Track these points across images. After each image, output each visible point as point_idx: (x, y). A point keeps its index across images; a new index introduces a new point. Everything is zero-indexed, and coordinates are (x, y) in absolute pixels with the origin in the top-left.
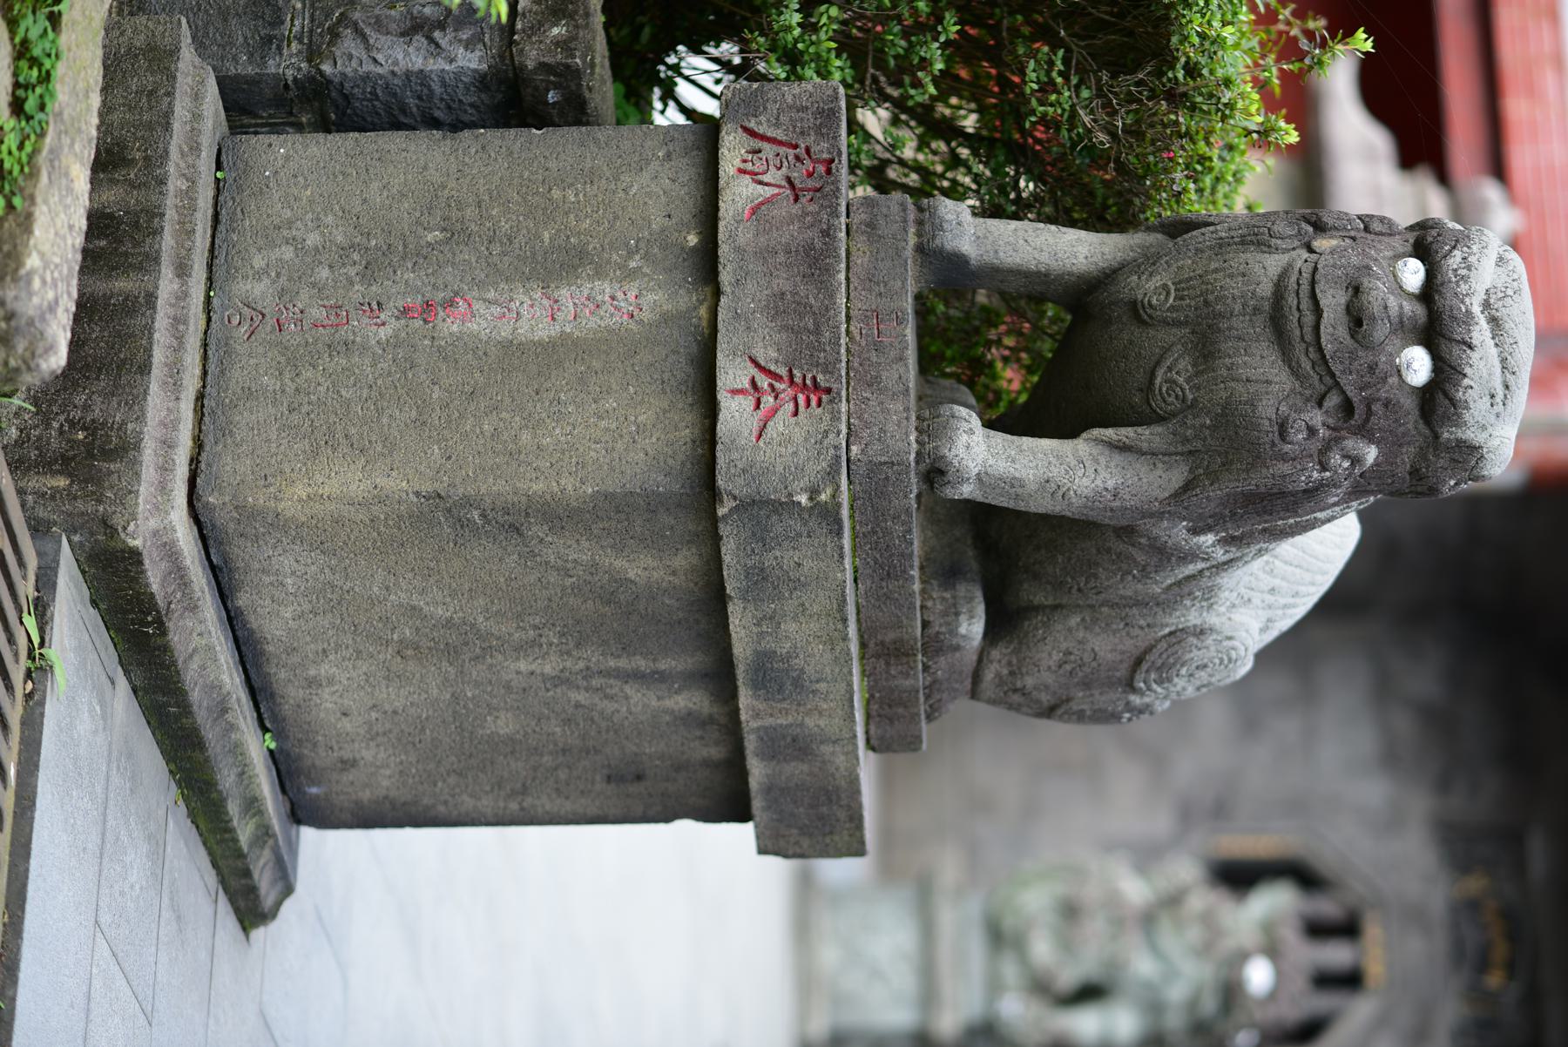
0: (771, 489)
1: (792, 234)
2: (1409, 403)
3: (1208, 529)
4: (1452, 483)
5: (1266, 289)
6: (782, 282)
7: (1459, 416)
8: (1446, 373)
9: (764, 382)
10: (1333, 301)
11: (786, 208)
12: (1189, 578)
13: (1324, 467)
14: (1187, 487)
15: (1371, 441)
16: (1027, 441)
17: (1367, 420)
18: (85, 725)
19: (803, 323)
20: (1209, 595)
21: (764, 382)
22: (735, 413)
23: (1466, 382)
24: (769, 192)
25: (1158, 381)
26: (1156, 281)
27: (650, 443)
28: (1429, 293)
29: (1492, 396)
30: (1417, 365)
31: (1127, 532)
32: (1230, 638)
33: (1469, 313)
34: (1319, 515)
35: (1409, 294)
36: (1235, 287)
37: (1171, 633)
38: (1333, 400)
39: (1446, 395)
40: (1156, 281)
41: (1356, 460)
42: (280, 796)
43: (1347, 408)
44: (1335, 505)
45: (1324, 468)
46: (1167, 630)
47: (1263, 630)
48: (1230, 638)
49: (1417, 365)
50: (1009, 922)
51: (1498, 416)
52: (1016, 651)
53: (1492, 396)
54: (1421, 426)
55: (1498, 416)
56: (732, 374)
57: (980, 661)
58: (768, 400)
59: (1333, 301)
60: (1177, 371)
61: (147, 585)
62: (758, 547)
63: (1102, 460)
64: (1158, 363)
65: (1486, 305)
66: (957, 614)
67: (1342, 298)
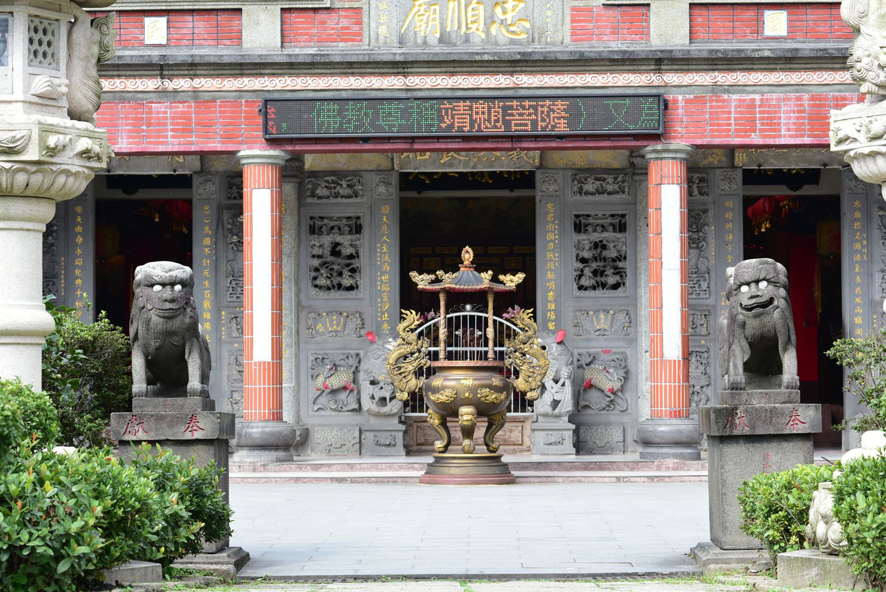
0: (217, 427)
1: (152, 424)
2: (185, 290)
5: (162, 320)
6: (165, 426)
9: (190, 429)
10: (168, 305)
11: (145, 425)
16: (190, 373)
18: (249, 571)
19: (174, 421)
21: (190, 429)
22: (198, 435)
24: (141, 429)
26: (153, 343)
27: (202, 454)
28: (164, 285)
30: (178, 287)
36: (160, 327)
40: (153, 343)
42: (632, 368)
50: (421, 399)
56: (188, 436)
58: (195, 428)
59: (168, 305)
60: (176, 340)
62: (783, 401)
67: (167, 303)
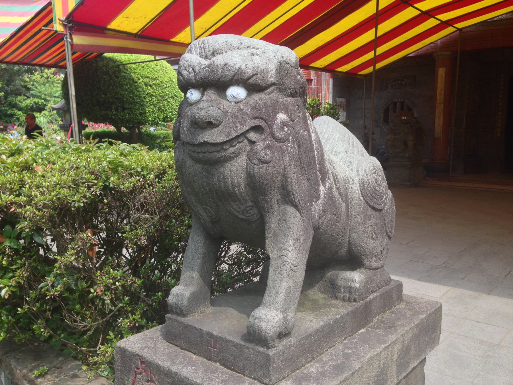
3: (317, 190)
4: (299, 77)
7: (262, 72)
8: (239, 79)
12: (340, 193)
13: (286, 140)
14: (296, 206)
15: (275, 116)
17: (263, 119)
20: (347, 181)
23: (243, 68)
25: (243, 217)
29: (253, 54)
30: (237, 92)
31: (316, 229)
32: (365, 171)
33: (209, 66)
34: (314, 138)
35: (245, 99)
37: (362, 196)
38: (252, 136)
39: (249, 78)
41: (284, 124)
43: (257, 129)
44: (309, 132)
45: (288, 140)
46: (362, 198)
47: (362, 155)
48: (365, 171)
49: (237, 92)
51: (263, 52)
52: (366, 256)
53: (253, 54)
54: (268, 91)
55: (263, 52)
57: (370, 269)
61: (328, 272)
63: (280, 246)
64: (236, 217)
65: (206, 58)
66: (351, 287)
